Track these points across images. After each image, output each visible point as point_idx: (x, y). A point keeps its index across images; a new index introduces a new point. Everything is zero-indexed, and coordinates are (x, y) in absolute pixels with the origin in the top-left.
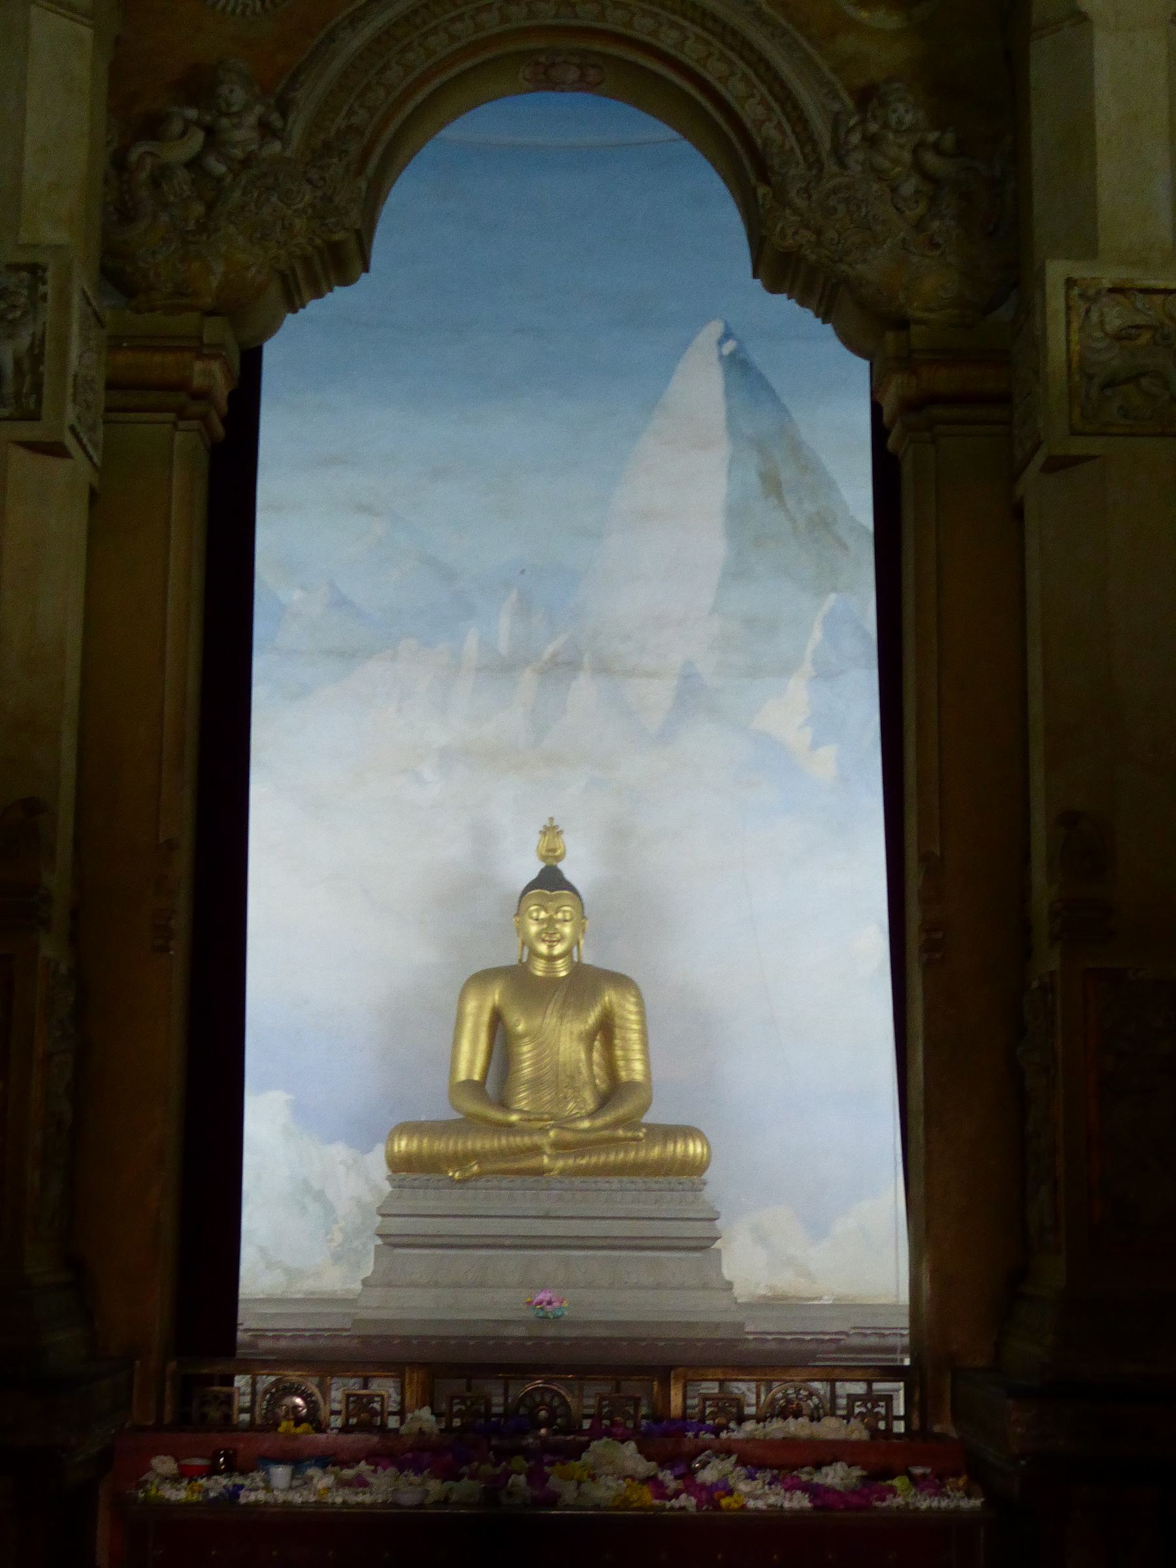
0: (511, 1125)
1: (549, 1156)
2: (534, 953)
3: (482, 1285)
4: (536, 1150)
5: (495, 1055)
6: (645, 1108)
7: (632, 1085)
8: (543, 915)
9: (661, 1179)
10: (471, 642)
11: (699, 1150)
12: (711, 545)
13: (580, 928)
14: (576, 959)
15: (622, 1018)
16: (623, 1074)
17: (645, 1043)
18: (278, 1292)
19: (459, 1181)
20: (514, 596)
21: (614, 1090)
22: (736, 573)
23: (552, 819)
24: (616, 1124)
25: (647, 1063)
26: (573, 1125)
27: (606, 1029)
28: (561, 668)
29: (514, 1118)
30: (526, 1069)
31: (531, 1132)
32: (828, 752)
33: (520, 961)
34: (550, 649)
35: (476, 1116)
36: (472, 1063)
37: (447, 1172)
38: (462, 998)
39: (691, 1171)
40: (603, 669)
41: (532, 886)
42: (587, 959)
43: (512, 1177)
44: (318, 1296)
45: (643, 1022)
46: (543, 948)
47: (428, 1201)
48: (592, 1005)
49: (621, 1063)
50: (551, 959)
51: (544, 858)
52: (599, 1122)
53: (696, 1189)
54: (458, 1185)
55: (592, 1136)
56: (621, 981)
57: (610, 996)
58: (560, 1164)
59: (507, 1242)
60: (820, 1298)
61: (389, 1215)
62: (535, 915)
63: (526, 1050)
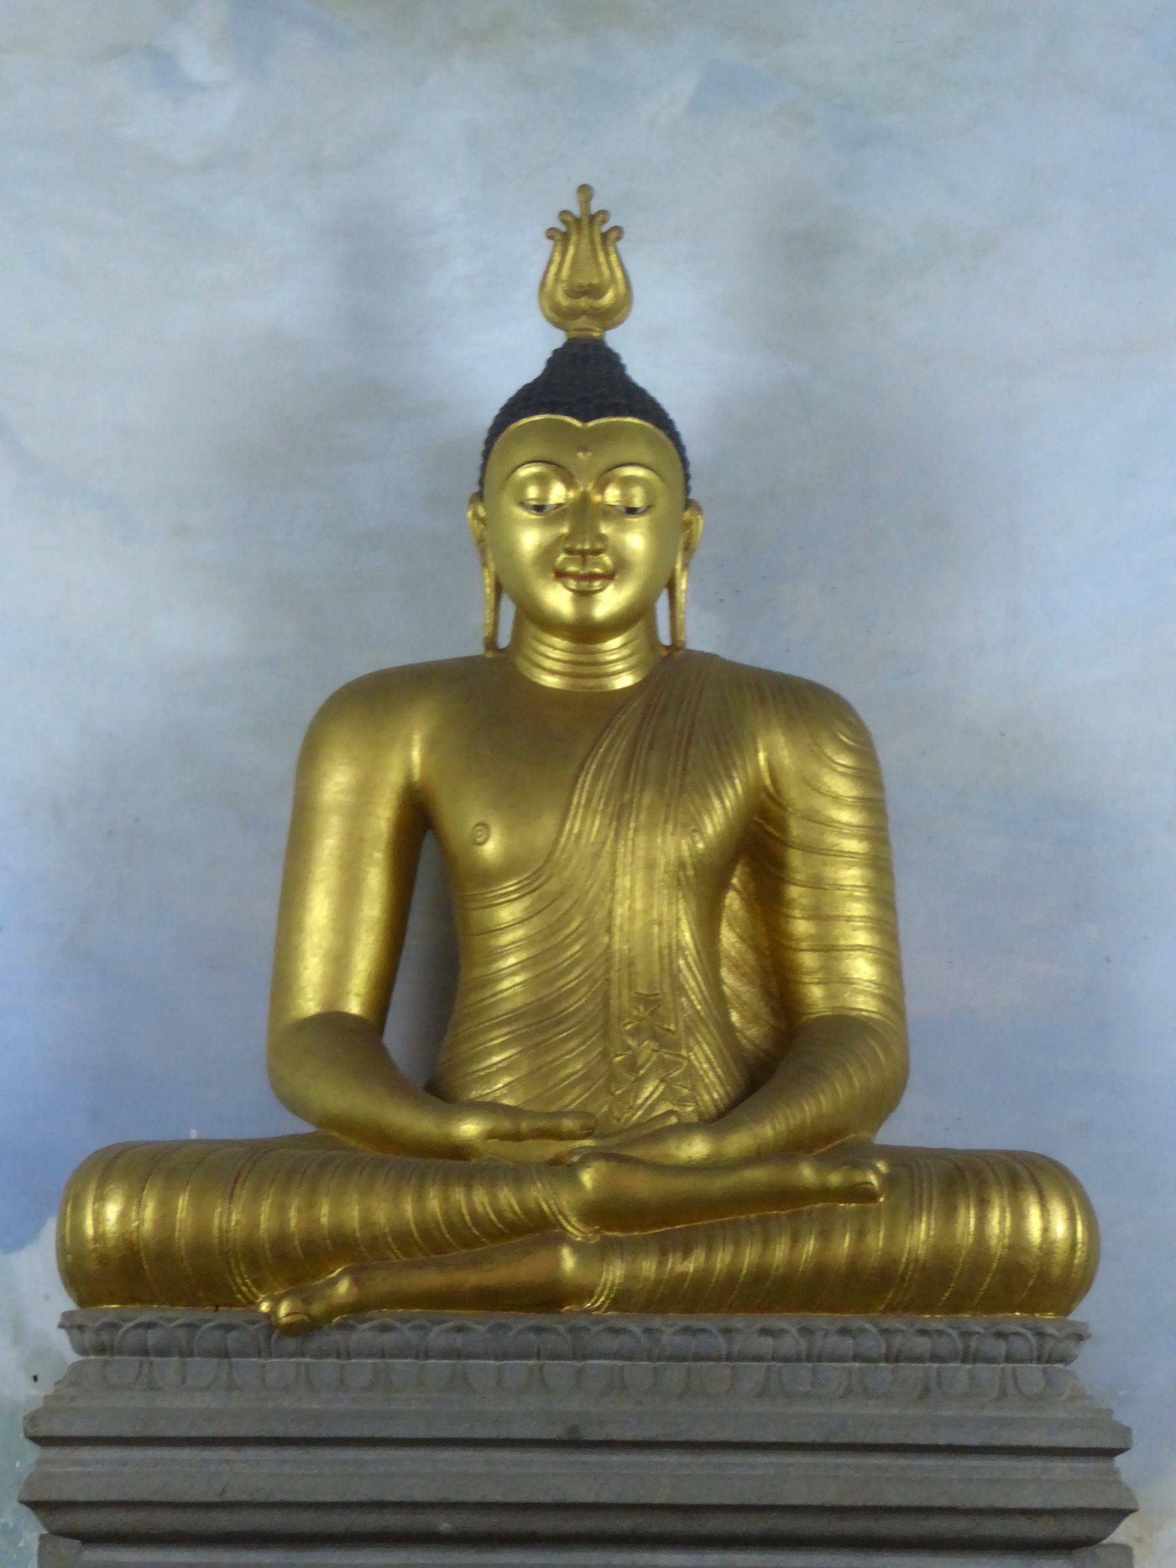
0: (458, 1152)
1: (577, 1248)
2: (535, 618)
4: (540, 1230)
5: (413, 942)
6: (884, 1101)
7: (845, 1028)
8: (558, 493)
11: (1060, 1228)
14: (665, 638)
15: (814, 819)
16: (816, 993)
17: (883, 898)
19: (290, 1330)
21: (786, 1044)
23: (585, 191)
24: (793, 1148)
25: (890, 957)
26: (654, 1152)
27: (761, 853)
29: (470, 1128)
30: (510, 977)
31: (518, 1174)
33: (491, 643)
36: (339, 961)
37: (252, 1303)
39: (1040, 1290)
45: (878, 832)
46: (559, 599)
47: (191, 1394)
49: (808, 960)
50: (586, 633)
51: (560, 317)
52: (738, 1142)
53: (1052, 1356)
54: (290, 1344)
55: (719, 1184)
57: (772, 752)
58: (615, 1273)
62: (532, 492)
63: (508, 914)
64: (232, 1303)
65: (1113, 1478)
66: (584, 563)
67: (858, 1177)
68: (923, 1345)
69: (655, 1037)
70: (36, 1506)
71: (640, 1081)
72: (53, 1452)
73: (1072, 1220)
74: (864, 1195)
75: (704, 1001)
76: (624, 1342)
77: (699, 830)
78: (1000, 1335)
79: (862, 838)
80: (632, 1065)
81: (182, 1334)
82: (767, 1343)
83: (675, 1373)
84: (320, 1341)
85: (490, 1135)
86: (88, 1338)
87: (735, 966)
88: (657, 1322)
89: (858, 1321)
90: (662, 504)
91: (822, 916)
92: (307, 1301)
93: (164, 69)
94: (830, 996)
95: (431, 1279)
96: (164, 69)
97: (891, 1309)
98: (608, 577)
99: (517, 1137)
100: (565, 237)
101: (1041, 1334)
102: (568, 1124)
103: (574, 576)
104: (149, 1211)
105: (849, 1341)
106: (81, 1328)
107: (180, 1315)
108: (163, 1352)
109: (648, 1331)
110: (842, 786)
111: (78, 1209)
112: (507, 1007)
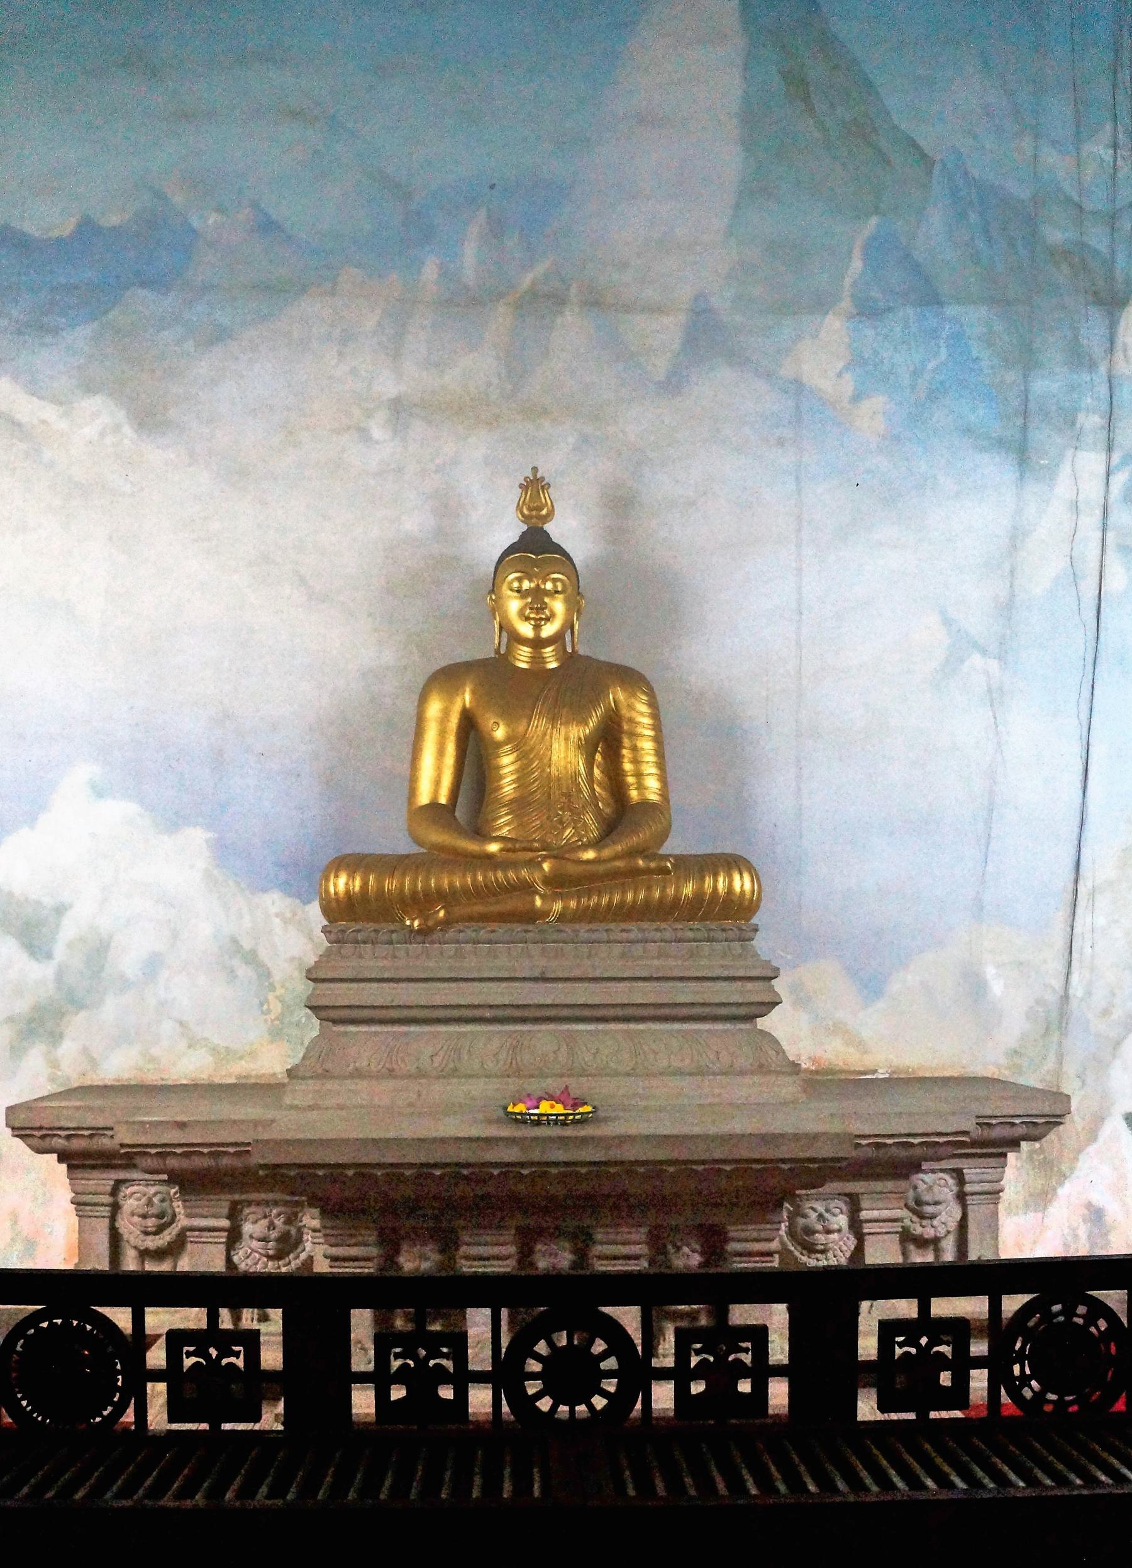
0: (490, 857)
1: (542, 897)
2: (517, 638)
3: (455, 1072)
4: (527, 889)
5: (466, 779)
6: (663, 836)
7: (646, 806)
8: (526, 585)
9: (696, 925)
10: (430, 272)
11: (747, 886)
12: (728, 160)
13: (574, 606)
14: (569, 650)
15: (631, 721)
16: (634, 794)
17: (660, 753)
18: (203, 1077)
19: (420, 931)
20: (482, 214)
21: (621, 813)
22: (755, 189)
23: (535, 469)
24: (632, 853)
25: (663, 779)
26: (573, 856)
27: (609, 740)
28: (544, 302)
29: (493, 848)
30: (508, 787)
31: (515, 865)
32: (878, 402)
33: (497, 651)
34: (527, 281)
35: (441, 848)
36: (437, 783)
37: (402, 921)
38: (423, 699)
39: (737, 913)
40: (594, 302)
41: (511, 549)
42: (582, 650)
43: (494, 926)
44: (253, 1081)
45: (657, 727)
46: (526, 630)
47: (373, 961)
48: (594, 702)
49: (631, 780)
50: (538, 644)
51: (526, 519)
52: (607, 853)
53: (746, 937)
54: (419, 938)
55: (601, 868)
56: (631, 678)
57: (617, 695)
58: (558, 906)
59: (488, 1014)
60: (875, 1071)
61: (324, 980)
62: (516, 585)
63: (507, 761)
64: (393, 921)
65: (772, 990)
66: (537, 614)
67: (663, 864)
68: (690, 934)
69: (570, 811)
70: (310, 1008)
71: (564, 829)
72: (320, 985)
73: (752, 881)
74: (664, 871)
75: (589, 796)
76: (563, 936)
77: (587, 724)
78: (723, 930)
79: (653, 729)
80: (561, 822)
81: (373, 935)
82: (625, 935)
83: (584, 949)
84: (437, 935)
85: (502, 850)
86: (333, 937)
87: (600, 784)
88: (577, 926)
89: (663, 925)
90: (569, 590)
91: (636, 761)
92: (426, 920)
93: (364, 434)
94: (639, 794)
95: (479, 909)
96: (364, 434)
97: (676, 920)
98: (548, 619)
99: (514, 851)
100: (527, 488)
101: (740, 929)
102: (536, 845)
103: (533, 619)
104: (358, 883)
105: (659, 934)
106: (330, 932)
107: (371, 926)
108: (365, 943)
109: (574, 931)
110: (644, 708)
111: (327, 880)
112: (508, 798)
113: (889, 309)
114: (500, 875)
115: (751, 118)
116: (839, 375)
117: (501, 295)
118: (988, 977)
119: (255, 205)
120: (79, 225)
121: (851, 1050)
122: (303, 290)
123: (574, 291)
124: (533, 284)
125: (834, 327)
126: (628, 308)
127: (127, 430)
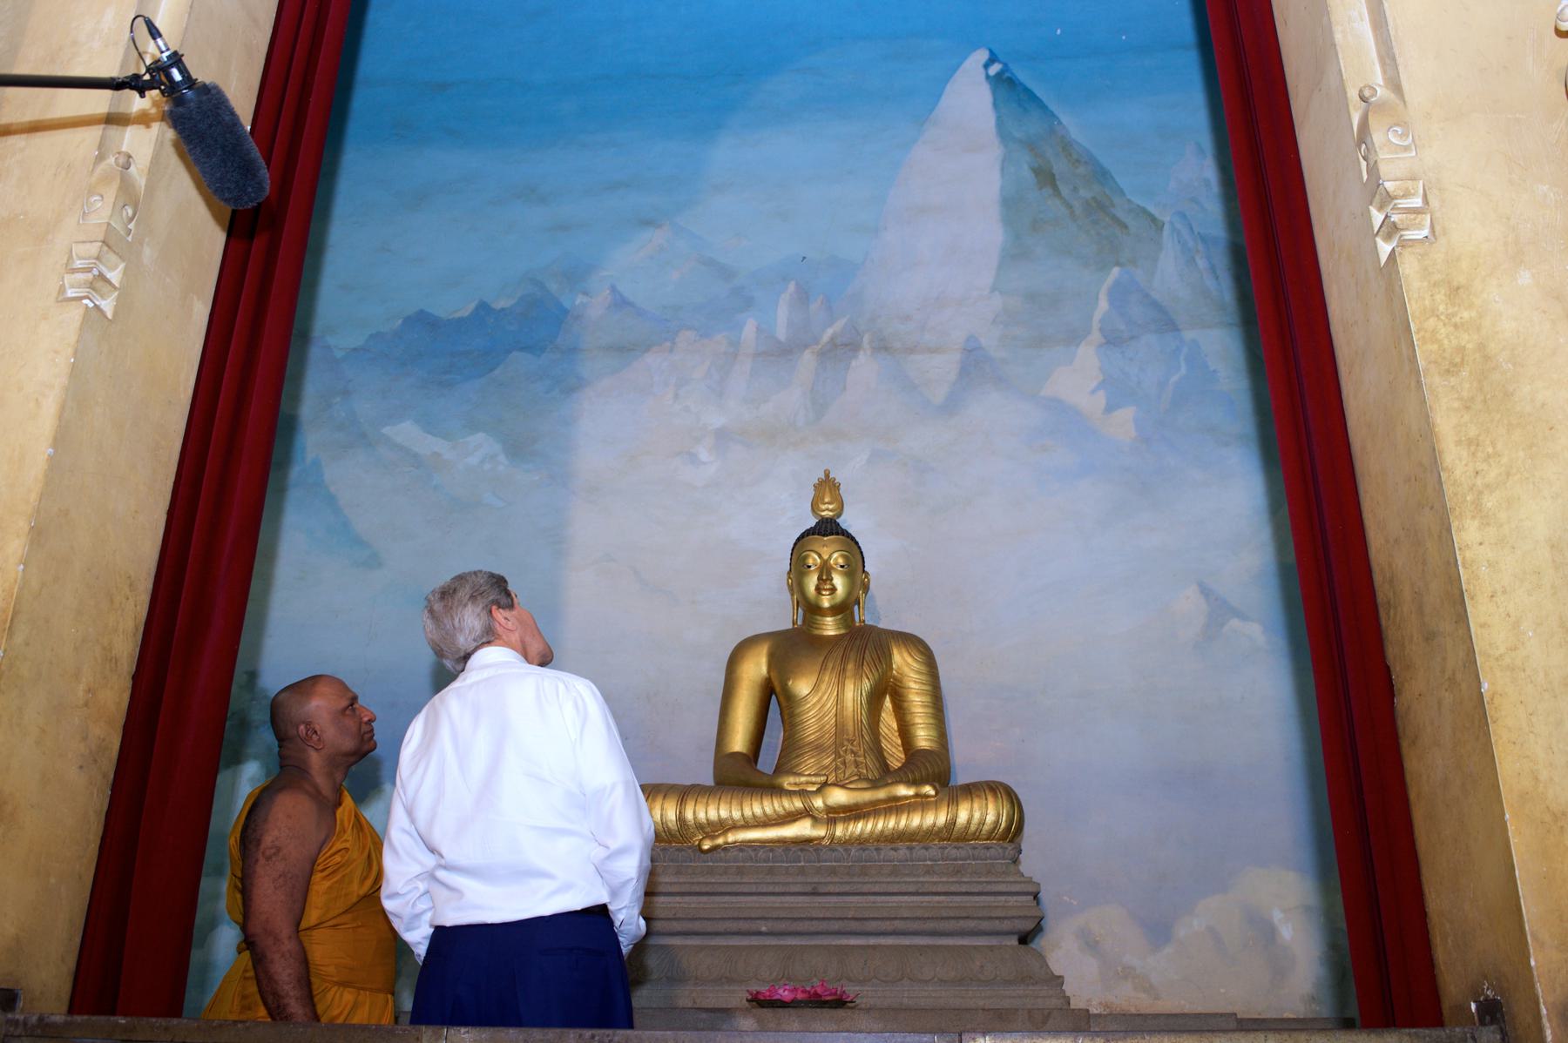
10: (749, 330)
20: (792, 287)
22: (1015, 254)
28: (843, 349)
34: (825, 338)
40: (883, 347)
93: (693, 459)
113: (1132, 338)
114: (748, 812)
115: (1011, 204)
116: (1093, 392)
117: (806, 346)
118: (1276, 921)
119: (613, 289)
120: (477, 308)
121: (1143, 996)
122: (647, 349)
123: (866, 339)
124: (832, 339)
125: (1087, 356)
126: (912, 350)
127: (502, 458)
